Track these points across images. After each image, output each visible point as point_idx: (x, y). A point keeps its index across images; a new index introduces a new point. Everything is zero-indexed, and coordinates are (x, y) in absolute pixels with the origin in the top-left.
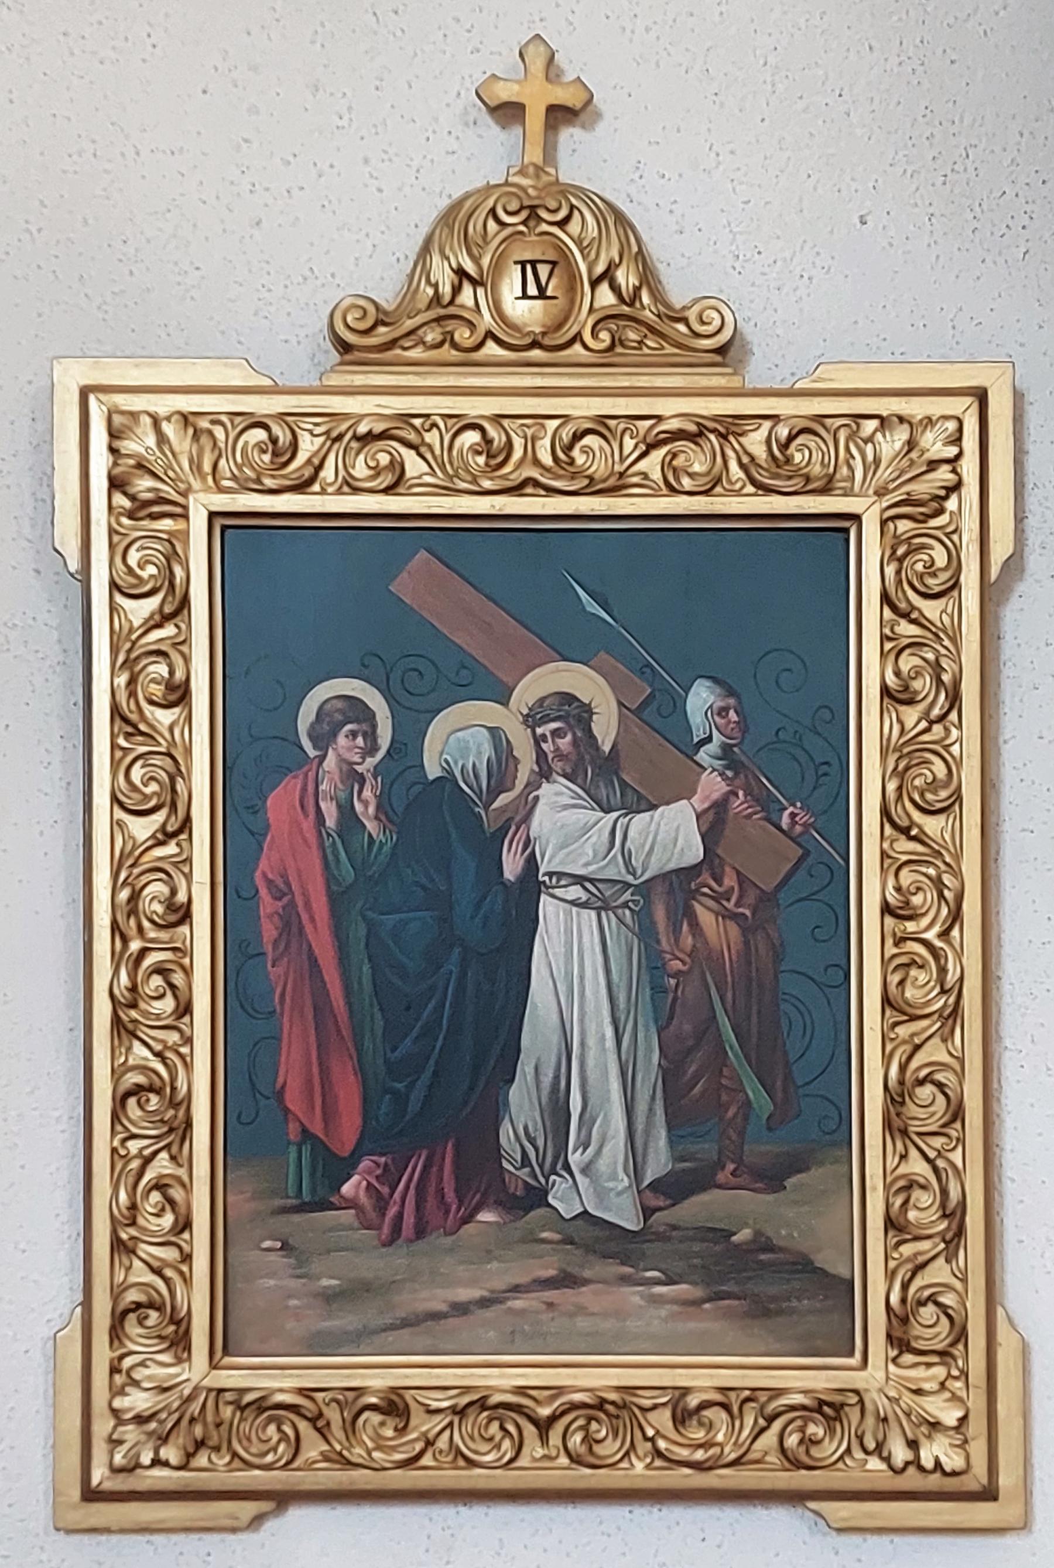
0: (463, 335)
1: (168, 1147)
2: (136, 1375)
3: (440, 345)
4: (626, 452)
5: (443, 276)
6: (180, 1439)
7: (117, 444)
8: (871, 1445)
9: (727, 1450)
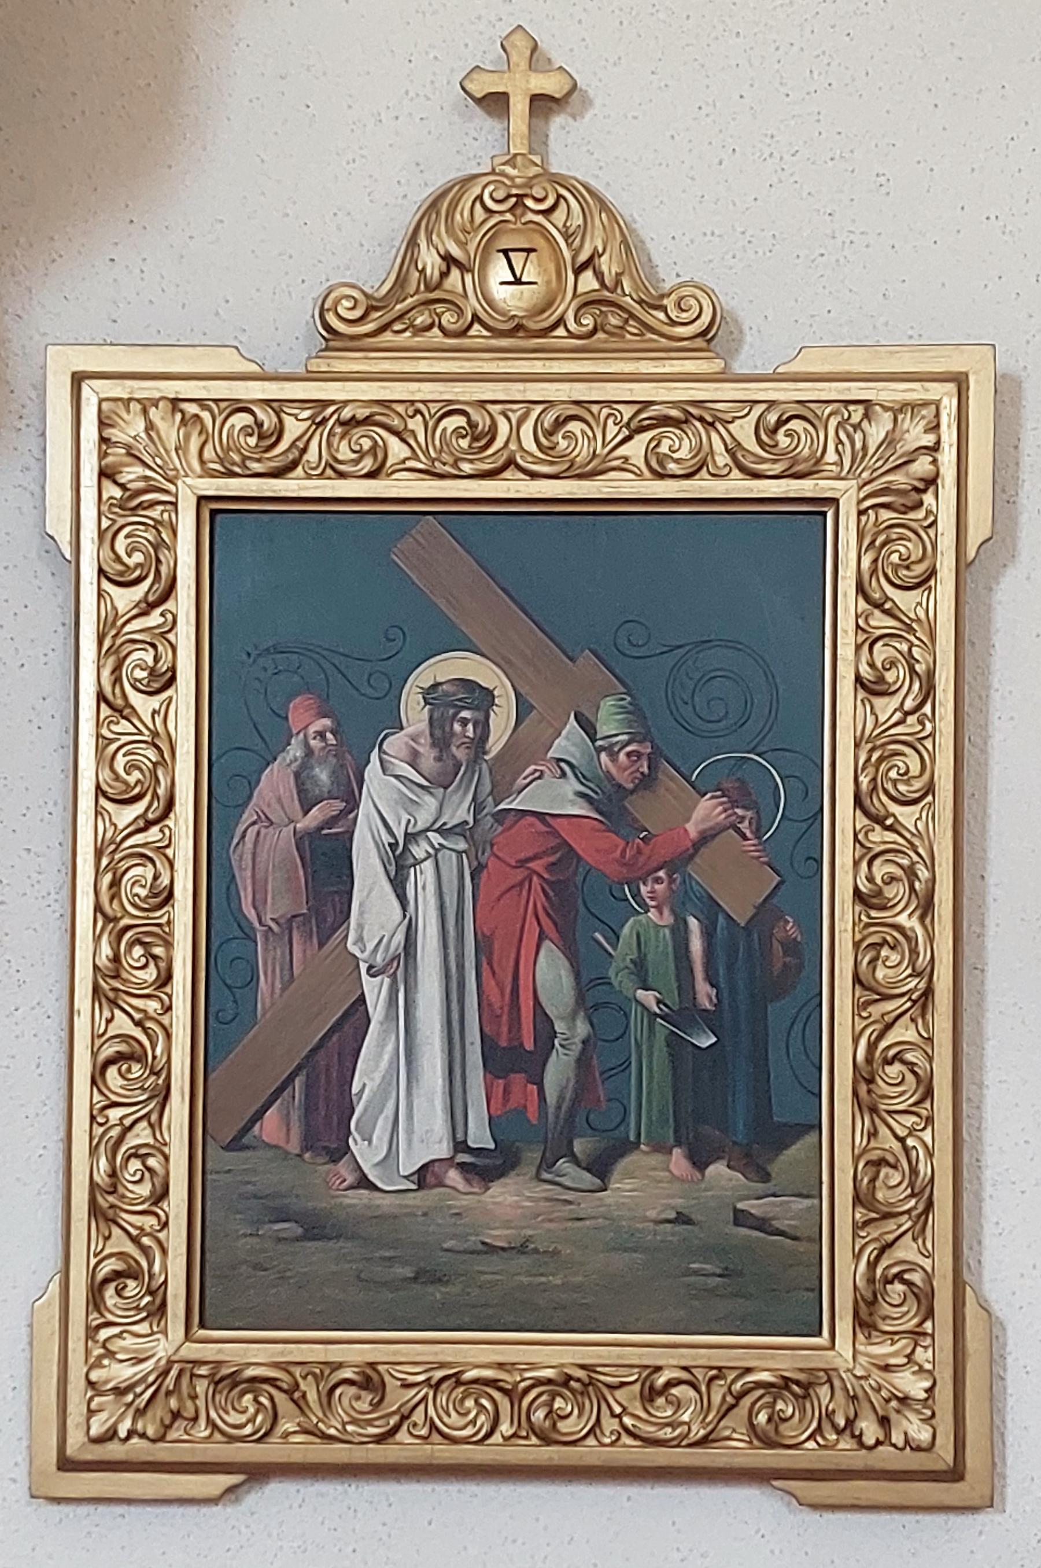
0: (448, 319)
1: (147, 1116)
2: (111, 1347)
3: (431, 327)
4: (609, 438)
5: (430, 261)
6: (159, 1411)
7: (108, 432)
8: (841, 1422)
9: (694, 1428)
